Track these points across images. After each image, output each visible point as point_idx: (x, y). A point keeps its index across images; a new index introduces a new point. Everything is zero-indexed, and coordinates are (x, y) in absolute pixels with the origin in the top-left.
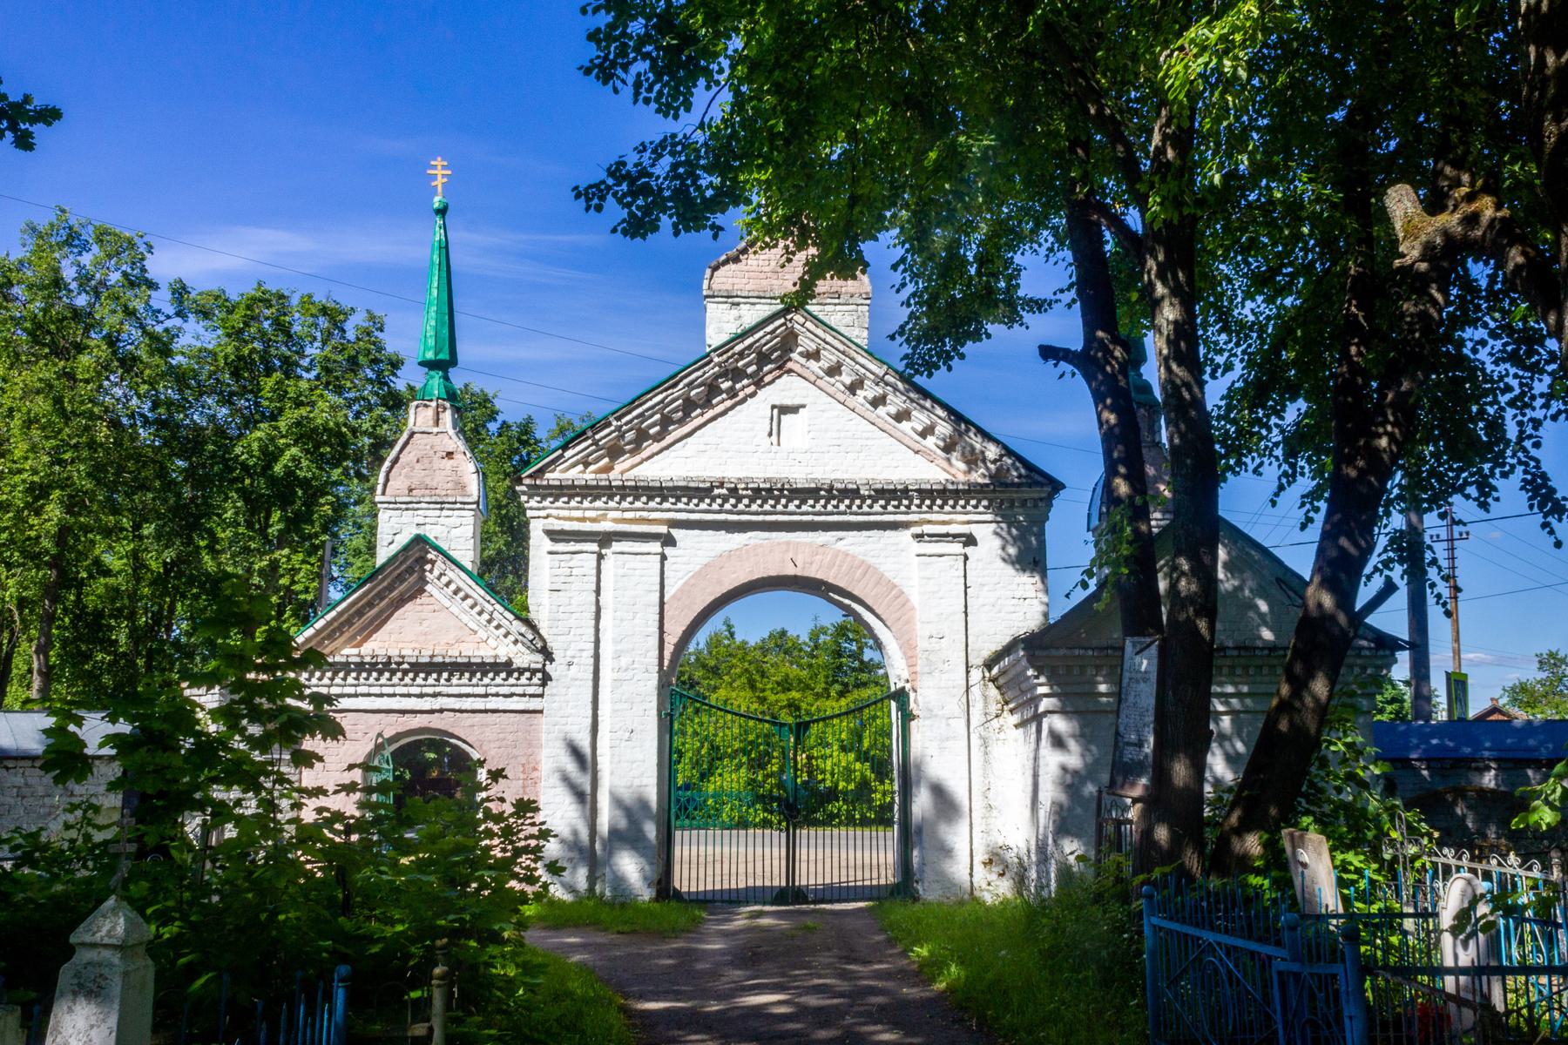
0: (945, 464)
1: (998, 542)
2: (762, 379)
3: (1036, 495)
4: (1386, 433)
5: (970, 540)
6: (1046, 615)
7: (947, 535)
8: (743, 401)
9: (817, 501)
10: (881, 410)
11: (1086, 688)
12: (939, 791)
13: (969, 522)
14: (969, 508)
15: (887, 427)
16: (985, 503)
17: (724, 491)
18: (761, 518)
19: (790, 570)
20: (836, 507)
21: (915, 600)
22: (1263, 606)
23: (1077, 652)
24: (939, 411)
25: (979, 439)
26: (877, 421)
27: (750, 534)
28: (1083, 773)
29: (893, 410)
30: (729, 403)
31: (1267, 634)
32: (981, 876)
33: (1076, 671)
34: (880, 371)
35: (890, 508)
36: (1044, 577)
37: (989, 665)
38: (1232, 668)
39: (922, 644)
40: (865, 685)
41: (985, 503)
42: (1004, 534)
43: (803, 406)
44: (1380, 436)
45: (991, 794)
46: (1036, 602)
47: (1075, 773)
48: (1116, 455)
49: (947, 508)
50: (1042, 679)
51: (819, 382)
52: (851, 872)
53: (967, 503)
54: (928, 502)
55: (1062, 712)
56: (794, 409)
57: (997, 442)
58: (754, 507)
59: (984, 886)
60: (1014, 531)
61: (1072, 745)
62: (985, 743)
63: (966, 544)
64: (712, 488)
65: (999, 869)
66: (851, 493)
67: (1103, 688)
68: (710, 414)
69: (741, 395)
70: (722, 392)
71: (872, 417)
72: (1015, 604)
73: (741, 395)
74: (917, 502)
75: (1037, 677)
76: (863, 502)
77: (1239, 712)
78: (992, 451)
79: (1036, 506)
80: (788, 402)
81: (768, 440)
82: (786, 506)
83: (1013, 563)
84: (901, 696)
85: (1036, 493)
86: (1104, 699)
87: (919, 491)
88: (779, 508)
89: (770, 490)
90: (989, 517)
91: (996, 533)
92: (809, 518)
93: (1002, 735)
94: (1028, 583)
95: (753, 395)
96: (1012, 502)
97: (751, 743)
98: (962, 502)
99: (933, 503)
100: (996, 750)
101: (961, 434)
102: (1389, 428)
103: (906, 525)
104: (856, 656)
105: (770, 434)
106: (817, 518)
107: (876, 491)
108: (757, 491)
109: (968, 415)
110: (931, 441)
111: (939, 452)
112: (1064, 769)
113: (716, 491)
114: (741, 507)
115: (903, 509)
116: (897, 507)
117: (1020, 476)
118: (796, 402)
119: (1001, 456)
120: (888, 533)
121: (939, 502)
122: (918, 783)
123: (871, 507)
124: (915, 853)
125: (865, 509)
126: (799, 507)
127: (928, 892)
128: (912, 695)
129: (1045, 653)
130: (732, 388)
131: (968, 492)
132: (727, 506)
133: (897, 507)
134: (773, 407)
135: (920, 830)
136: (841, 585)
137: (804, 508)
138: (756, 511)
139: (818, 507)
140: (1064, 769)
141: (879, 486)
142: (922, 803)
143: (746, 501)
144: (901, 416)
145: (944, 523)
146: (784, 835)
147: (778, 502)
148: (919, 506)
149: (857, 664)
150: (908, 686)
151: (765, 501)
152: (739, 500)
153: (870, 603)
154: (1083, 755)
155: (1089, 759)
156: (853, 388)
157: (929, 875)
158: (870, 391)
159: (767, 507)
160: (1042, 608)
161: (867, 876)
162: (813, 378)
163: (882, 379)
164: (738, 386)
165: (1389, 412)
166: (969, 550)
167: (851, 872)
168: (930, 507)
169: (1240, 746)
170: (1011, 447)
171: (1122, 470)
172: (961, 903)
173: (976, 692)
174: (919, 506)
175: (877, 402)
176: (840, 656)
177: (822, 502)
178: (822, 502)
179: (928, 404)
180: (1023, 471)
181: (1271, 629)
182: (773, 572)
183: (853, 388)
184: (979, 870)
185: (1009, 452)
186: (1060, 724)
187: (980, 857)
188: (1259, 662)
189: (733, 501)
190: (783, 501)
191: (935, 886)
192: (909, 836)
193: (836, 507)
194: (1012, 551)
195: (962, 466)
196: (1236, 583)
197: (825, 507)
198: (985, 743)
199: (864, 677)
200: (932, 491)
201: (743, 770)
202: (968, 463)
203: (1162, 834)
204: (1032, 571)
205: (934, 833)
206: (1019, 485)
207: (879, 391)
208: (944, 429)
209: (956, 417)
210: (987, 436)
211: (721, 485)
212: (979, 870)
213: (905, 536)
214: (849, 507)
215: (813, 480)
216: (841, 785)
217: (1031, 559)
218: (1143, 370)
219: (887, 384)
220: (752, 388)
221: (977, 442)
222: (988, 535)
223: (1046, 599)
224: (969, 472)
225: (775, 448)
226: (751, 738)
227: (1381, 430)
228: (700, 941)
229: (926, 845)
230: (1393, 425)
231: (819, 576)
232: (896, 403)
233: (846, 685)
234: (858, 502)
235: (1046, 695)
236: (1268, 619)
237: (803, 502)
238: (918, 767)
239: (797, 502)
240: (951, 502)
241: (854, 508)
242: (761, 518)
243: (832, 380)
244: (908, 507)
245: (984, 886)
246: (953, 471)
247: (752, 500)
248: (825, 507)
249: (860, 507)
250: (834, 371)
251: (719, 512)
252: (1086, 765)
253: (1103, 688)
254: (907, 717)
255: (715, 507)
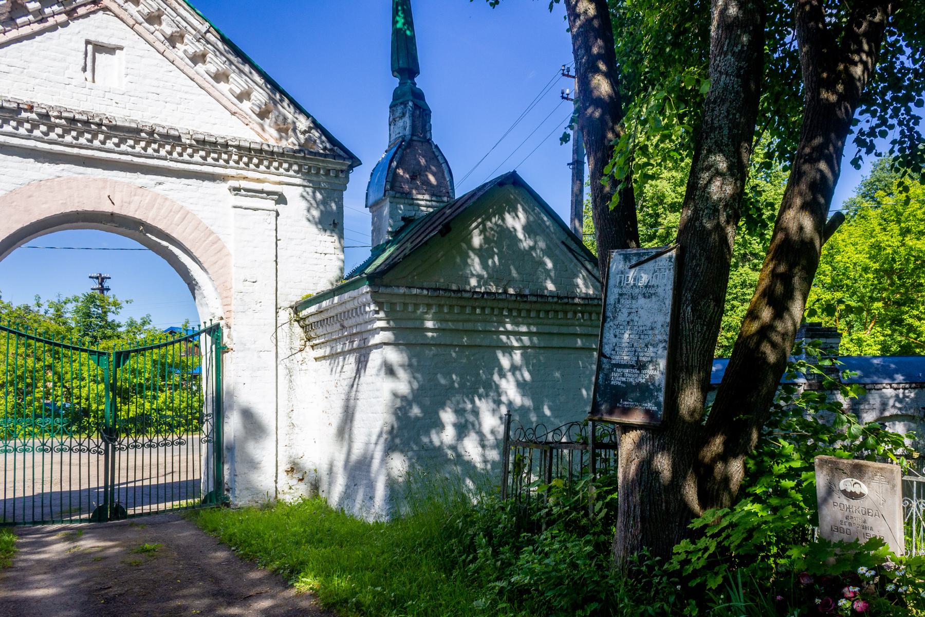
0: (259, 129)
1: (304, 204)
2: (74, 10)
3: (338, 167)
4: (861, 61)
5: (281, 199)
6: (342, 270)
7: (262, 192)
8: (53, 28)
9: (137, 142)
10: (200, 68)
11: (417, 324)
12: (248, 415)
13: (280, 183)
14: (281, 170)
15: (205, 85)
16: (295, 167)
17: (34, 116)
18: (75, 151)
19: (107, 208)
20: (157, 151)
21: (231, 246)
22: (550, 265)
23: (415, 291)
24: (256, 77)
25: (292, 109)
26: (196, 77)
27: (62, 166)
28: (410, 397)
29: (213, 69)
30: (36, 27)
31: (551, 286)
32: (284, 480)
33: (410, 308)
34: (204, 28)
35: (210, 160)
36: (341, 237)
37: (296, 308)
38: (529, 311)
39: (237, 286)
40: (110, 337)
41: (295, 167)
42: (309, 198)
43: (121, 48)
44: (855, 64)
45: (294, 415)
46: (334, 257)
47: (404, 398)
48: (595, 50)
49: (262, 168)
50: (382, 315)
51: (137, 27)
52: (131, 474)
53: (280, 165)
54: (245, 159)
55: (394, 344)
56: (111, 50)
57: (308, 116)
58: (68, 139)
59: (286, 490)
60: (319, 196)
61: (402, 374)
62: (290, 373)
63: (278, 202)
64: (19, 110)
65: (298, 475)
66: (174, 140)
67: (429, 324)
68: (13, 34)
69: (51, 21)
70: (27, 13)
71: (191, 72)
72: (318, 261)
73: (51, 21)
74: (235, 157)
75: (377, 312)
76: (184, 149)
77: (528, 347)
78: (303, 123)
79: (337, 176)
80: (104, 40)
81: (82, 75)
82: (103, 143)
83: (316, 224)
84: (214, 331)
85: (334, 164)
86: (430, 334)
87: (239, 147)
88: (96, 143)
89: (87, 123)
90: (298, 181)
91: (303, 197)
92: (128, 158)
93: (304, 367)
94: (328, 241)
95: (65, 25)
96: (318, 170)
97: (18, 377)
98: (276, 164)
99: (250, 160)
100: (299, 379)
101: (275, 103)
102: (864, 57)
103: (224, 178)
104: (103, 317)
105: (84, 69)
106: (136, 160)
107: (197, 141)
108: (73, 121)
109: (283, 86)
110: (246, 105)
111: (254, 116)
112: (395, 395)
113: (24, 115)
114: (53, 136)
115: (221, 162)
116: (216, 160)
117: (325, 149)
118: (113, 42)
119: (310, 128)
120: (207, 183)
121: (255, 161)
122: (231, 407)
123: (191, 156)
124: (226, 467)
125: (186, 157)
126: (118, 145)
127: (240, 499)
128: (225, 331)
129: (389, 290)
130: (40, 11)
131: (282, 154)
132: (37, 133)
133: (216, 160)
134: (88, 42)
135: (231, 449)
136: (161, 226)
137: (123, 147)
138: (69, 143)
139: (138, 149)
140: (395, 395)
141: (201, 137)
142: (232, 426)
143: (59, 131)
144: (219, 77)
145: (258, 180)
146: (102, 458)
147: (95, 136)
148: (237, 162)
149: (103, 323)
150: (222, 323)
151: (81, 134)
152: (51, 128)
153: (188, 245)
154: (410, 382)
155: (416, 385)
156: (173, 40)
157: (238, 487)
158: (191, 46)
159: (82, 141)
160: (340, 264)
161: (146, 475)
162: (131, 22)
163: (203, 37)
164: (48, 11)
165: (864, 41)
166: (280, 207)
167: (131, 474)
168: (247, 164)
169: (527, 376)
170: (319, 121)
171: (602, 67)
172: (267, 506)
173: (283, 332)
174: (237, 162)
175: (198, 59)
176: (90, 317)
177: (143, 144)
178: (143, 144)
179: (247, 68)
180: (328, 145)
181: (553, 282)
182: (89, 207)
183: (173, 40)
184: (282, 476)
185: (317, 126)
186: (393, 356)
187: (284, 466)
188: (548, 307)
189: (43, 128)
190: (101, 137)
191: (245, 492)
192: (219, 451)
193: (157, 151)
194: (316, 213)
195: (275, 133)
196: (531, 244)
197: (145, 149)
198: (290, 373)
199: (109, 332)
200: (250, 149)
201: (10, 397)
202: (279, 130)
203: (663, 464)
204: (332, 231)
205: (243, 449)
206: (325, 156)
207: (200, 47)
208: (260, 96)
209: (274, 86)
210: (299, 109)
211: (31, 109)
212: (282, 476)
213: (222, 188)
214: (170, 153)
215: (132, 121)
216: (94, 406)
217: (332, 222)
218: (416, 79)
219: (208, 42)
220: (63, 18)
221: (288, 112)
222: (297, 195)
223: (342, 257)
224: (281, 138)
225: (89, 84)
226: (19, 373)
227: (856, 58)
228: (23, 584)
229: (238, 459)
230: (868, 54)
231: (138, 216)
232: (215, 63)
233: (95, 337)
234: (179, 149)
235: (383, 329)
236: (552, 274)
237: (123, 141)
238: (231, 395)
239: (116, 140)
240: (266, 163)
241: (175, 155)
242: (75, 151)
243: (152, 28)
244: (227, 161)
245: (286, 490)
246: (266, 136)
247: (67, 131)
248: (145, 149)
249: (181, 155)
250: (154, 18)
251: (28, 138)
252: (412, 390)
253: (429, 324)
254: (221, 350)
255: (22, 131)
